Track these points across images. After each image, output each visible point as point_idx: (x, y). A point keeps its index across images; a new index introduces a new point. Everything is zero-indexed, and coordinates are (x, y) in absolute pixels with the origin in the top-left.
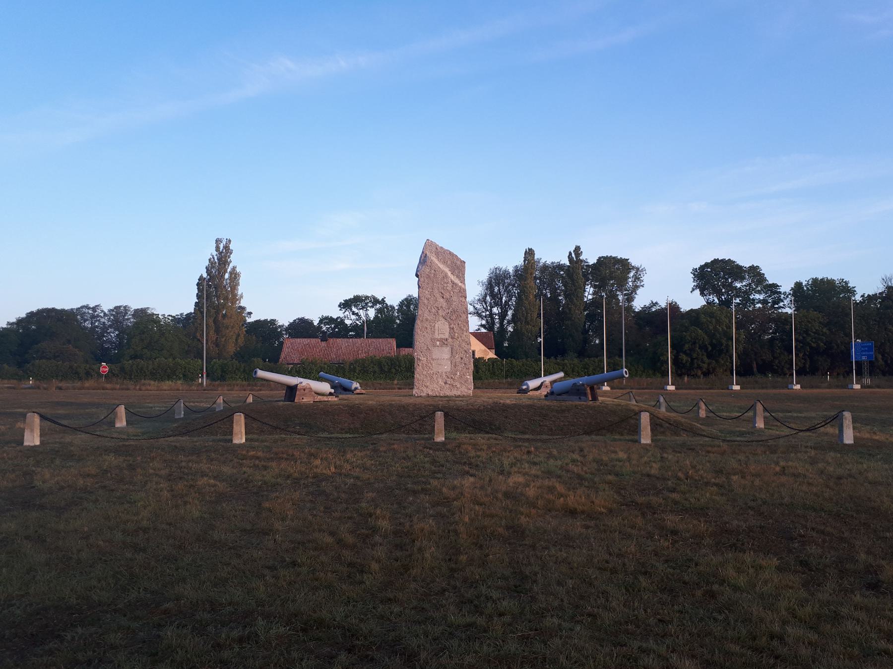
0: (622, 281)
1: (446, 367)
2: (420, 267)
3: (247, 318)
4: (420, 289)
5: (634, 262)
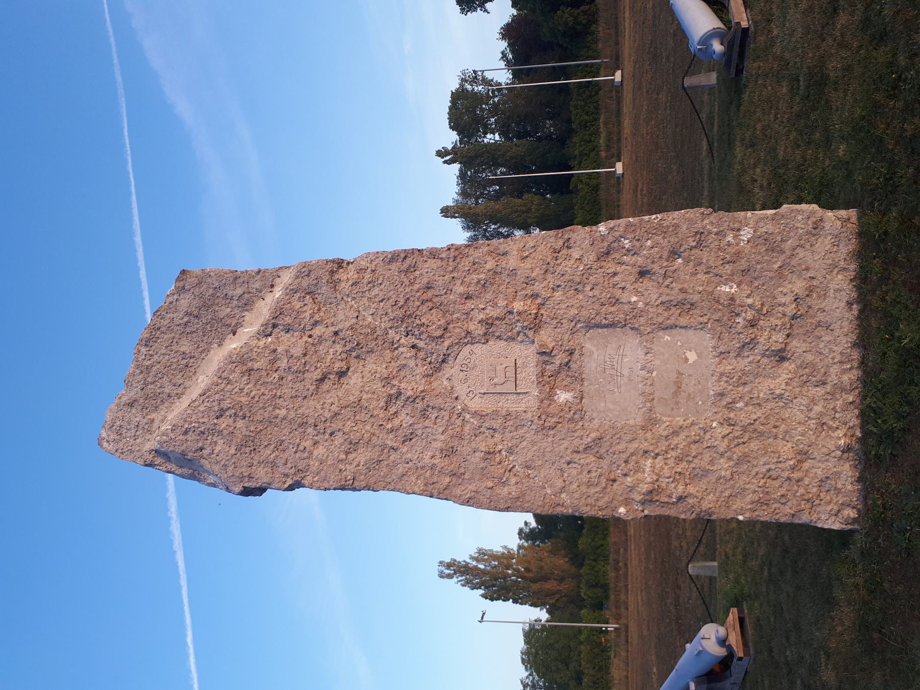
0: (477, 99)
1: (692, 357)
2: (211, 479)
3: (531, 527)
4: (305, 482)
5: (455, 85)
